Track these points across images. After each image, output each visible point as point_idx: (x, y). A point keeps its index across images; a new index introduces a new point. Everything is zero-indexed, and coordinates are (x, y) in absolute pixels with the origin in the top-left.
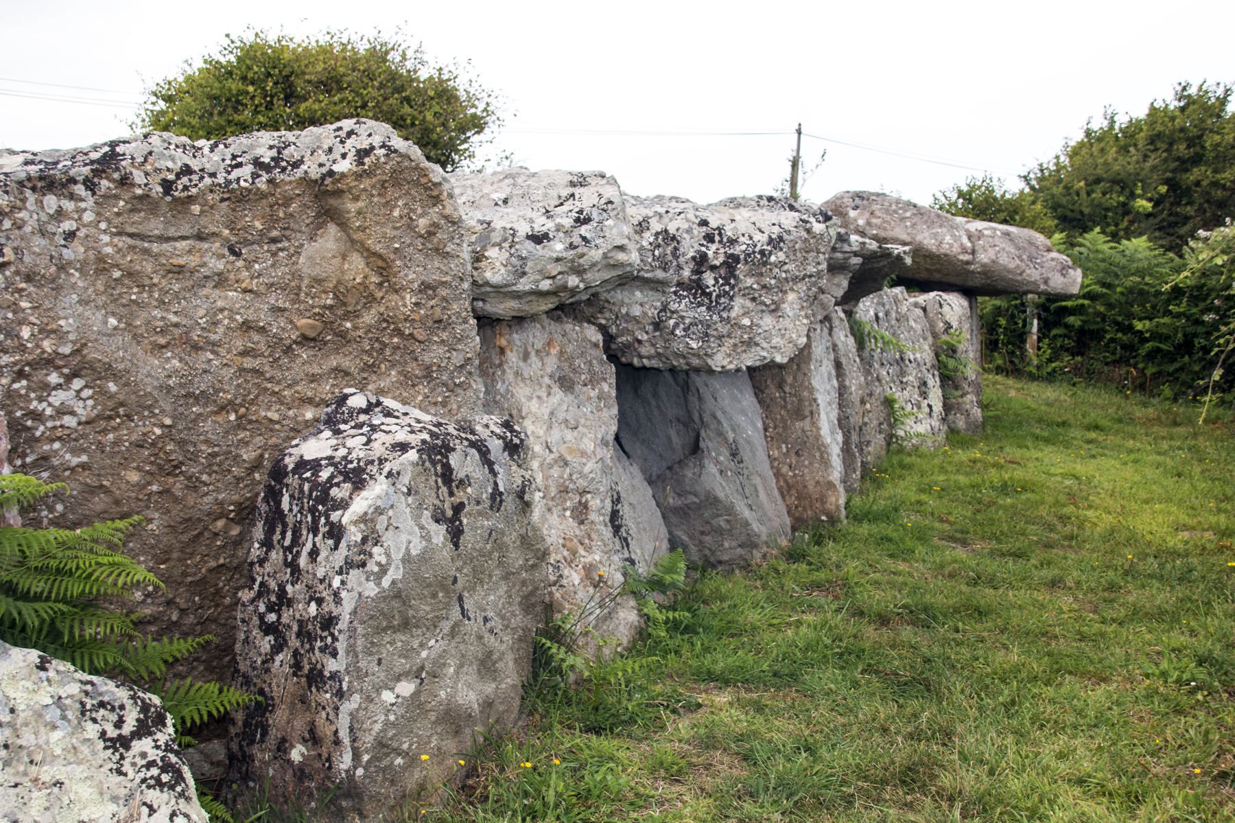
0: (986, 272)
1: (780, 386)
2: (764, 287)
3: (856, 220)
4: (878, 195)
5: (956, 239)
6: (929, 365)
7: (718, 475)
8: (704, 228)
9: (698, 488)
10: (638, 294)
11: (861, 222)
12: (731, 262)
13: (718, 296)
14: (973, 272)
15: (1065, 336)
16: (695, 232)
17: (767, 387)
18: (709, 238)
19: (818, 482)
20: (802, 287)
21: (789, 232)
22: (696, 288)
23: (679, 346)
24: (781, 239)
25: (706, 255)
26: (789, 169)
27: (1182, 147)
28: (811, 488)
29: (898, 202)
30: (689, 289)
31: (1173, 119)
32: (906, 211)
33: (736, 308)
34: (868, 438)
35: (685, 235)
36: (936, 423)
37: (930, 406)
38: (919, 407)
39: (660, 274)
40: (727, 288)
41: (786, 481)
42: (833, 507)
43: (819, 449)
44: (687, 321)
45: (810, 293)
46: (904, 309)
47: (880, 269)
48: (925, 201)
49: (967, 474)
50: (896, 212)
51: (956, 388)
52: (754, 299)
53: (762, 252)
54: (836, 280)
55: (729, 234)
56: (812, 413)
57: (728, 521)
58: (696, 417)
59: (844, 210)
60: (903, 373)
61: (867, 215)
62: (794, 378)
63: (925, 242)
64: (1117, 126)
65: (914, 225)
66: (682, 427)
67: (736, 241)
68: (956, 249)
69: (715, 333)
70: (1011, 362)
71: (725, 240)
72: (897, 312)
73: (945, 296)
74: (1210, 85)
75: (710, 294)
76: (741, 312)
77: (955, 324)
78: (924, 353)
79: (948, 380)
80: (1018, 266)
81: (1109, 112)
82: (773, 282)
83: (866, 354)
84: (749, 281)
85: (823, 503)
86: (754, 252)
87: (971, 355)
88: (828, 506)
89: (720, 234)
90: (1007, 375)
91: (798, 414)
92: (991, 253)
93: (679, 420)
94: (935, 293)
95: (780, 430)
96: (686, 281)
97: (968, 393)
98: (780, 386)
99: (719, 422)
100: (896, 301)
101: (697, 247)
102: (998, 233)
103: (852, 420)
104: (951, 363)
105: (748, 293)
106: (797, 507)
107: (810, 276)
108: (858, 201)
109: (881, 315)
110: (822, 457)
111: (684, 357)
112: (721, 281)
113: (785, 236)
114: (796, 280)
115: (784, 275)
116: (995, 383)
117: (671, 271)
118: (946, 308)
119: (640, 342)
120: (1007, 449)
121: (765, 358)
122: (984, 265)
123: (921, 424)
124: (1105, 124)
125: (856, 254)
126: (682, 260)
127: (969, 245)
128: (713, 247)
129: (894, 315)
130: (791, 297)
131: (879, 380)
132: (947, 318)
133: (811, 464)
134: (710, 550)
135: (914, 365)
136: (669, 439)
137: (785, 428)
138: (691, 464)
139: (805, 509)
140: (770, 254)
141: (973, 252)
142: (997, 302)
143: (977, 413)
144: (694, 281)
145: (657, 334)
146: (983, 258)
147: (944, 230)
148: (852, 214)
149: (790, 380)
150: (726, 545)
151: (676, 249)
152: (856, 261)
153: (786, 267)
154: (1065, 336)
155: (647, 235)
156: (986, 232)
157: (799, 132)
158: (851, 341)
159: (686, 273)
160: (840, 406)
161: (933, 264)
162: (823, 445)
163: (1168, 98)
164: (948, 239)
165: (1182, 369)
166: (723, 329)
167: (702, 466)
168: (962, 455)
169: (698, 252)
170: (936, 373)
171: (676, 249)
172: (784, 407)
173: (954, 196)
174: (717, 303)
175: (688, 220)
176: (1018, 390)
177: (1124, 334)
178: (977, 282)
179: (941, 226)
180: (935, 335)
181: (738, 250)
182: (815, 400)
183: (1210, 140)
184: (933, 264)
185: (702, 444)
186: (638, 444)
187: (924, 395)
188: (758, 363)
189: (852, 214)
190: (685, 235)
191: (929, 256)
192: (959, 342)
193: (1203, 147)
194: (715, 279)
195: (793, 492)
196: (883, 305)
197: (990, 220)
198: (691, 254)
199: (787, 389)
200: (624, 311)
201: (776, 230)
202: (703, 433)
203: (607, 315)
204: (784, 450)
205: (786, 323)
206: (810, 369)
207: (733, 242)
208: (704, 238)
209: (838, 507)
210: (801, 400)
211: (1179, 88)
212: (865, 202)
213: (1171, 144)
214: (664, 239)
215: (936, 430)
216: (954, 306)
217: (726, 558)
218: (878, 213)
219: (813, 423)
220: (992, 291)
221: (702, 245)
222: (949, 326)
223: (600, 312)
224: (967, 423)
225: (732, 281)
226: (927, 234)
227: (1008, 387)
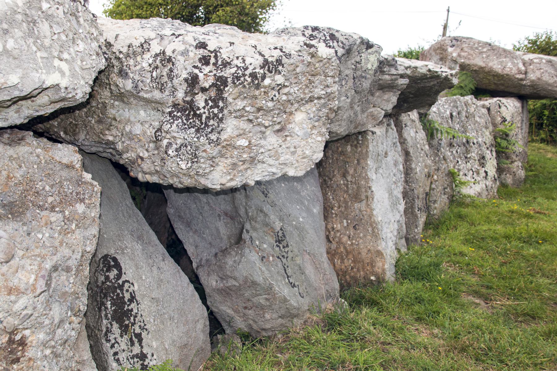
0: (534, 85)
1: (344, 176)
2: (259, 109)
3: (452, 54)
4: (468, 38)
6: (488, 145)
7: (258, 263)
8: (202, 50)
9: (236, 274)
10: (142, 113)
11: (455, 55)
12: (221, 83)
13: (208, 118)
14: (525, 85)
16: (191, 54)
17: (334, 176)
18: (205, 61)
19: (369, 250)
20: (312, 108)
21: (288, 56)
22: (188, 109)
23: (171, 165)
24: (279, 62)
25: (197, 76)
26: (442, 30)
28: (364, 254)
29: (479, 42)
30: (183, 110)
32: (484, 48)
33: (229, 130)
34: (435, 198)
35: (179, 57)
36: (489, 183)
37: (486, 172)
38: (478, 173)
39: (157, 95)
40: (216, 111)
41: (345, 248)
42: (380, 271)
43: (371, 225)
44: (179, 142)
45: (321, 114)
46: (472, 110)
47: (431, 88)
48: (509, 47)
49: (505, 224)
50: (477, 48)
51: (507, 158)
52: (250, 121)
53: (253, 76)
54: (386, 97)
55: (224, 56)
56: (367, 197)
57: (266, 299)
58: (242, 212)
59: (445, 48)
60: (468, 151)
61: (459, 50)
62: (355, 170)
63: (494, 67)
66: (229, 220)
67: (229, 64)
68: (514, 71)
69: (204, 154)
70: (551, 136)
71: (220, 63)
72: (467, 112)
73: (503, 100)
75: (200, 116)
76: (236, 133)
77: (508, 119)
78: (487, 137)
79: (502, 154)
82: (270, 104)
83: (435, 142)
84: (240, 104)
85: (373, 266)
86: (244, 75)
87: (520, 136)
88: (376, 269)
89: (216, 57)
90: (547, 144)
91: (357, 198)
92: (538, 74)
93: (226, 214)
94: (498, 98)
95: (343, 209)
96: (181, 102)
97: (515, 161)
98: (344, 176)
99: (266, 215)
100: (466, 104)
101: (189, 70)
102: (544, 61)
103: (416, 192)
104: (504, 143)
105: (240, 114)
106: (352, 268)
107: (319, 98)
108: (454, 42)
109: (454, 114)
110: (373, 231)
111: (178, 177)
112: (211, 104)
113: (285, 60)
114: (302, 102)
115: (284, 98)
116: (539, 149)
117: (167, 93)
118: (503, 109)
119: (142, 159)
120: (539, 200)
121: (274, 174)
122: (532, 81)
123: (476, 185)
125: (402, 76)
126: (175, 81)
127: (523, 68)
128: (206, 69)
129: (464, 114)
130: (299, 117)
131: (444, 159)
132: (504, 115)
133: (365, 236)
134: (254, 321)
135: (476, 146)
136: (218, 230)
137: (346, 208)
138: (233, 253)
139: (358, 270)
140: (264, 77)
141: (526, 73)
142: (544, 101)
143: (522, 173)
144: (188, 102)
145: (156, 152)
146: (532, 76)
147: (508, 59)
148: (450, 50)
149: (351, 171)
150: (267, 316)
151: (171, 70)
152: (404, 82)
153: (286, 90)
155: (147, 56)
156: (535, 61)
157: (448, 11)
158: (422, 135)
159: (180, 95)
160: (406, 182)
161: (499, 80)
162: (374, 222)
164: (509, 65)
166: (213, 151)
167: (242, 255)
168: (506, 206)
169: (190, 74)
170: (493, 149)
171: (171, 70)
172: (347, 192)
173: (526, 43)
174: (207, 125)
175: (184, 42)
176: (553, 153)
178: (527, 91)
179: (505, 57)
180: (495, 125)
181: (228, 73)
182: (370, 188)
185: (245, 236)
186: (191, 234)
187: (483, 165)
188: (267, 178)
189: (450, 50)
190: (179, 57)
191: (496, 76)
192: (511, 130)
194: (206, 101)
195: (350, 256)
196: (457, 108)
197: (549, 55)
198: (184, 75)
199: (349, 178)
200: (128, 129)
201: (277, 54)
202: (247, 226)
203: (114, 132)
204: (345, 224)
205: (295, 141)
206: (367, 164)
207: (226, 64)
208: (200, 60)
209: (384, 270)
210: (359, 188)
212: (459, 43)
214: (161, 61)
215: (489, 188)
216: (510, 107)
217: (268, 326)
218: (466, 49)
219: (368, 205)
220: (537, 96)
221: (195, 67)
222: (504, 120)
223: (109, 129)
224: (513, 180)
225: (221, 104)
226: (495, 62)
227: (547, 151)
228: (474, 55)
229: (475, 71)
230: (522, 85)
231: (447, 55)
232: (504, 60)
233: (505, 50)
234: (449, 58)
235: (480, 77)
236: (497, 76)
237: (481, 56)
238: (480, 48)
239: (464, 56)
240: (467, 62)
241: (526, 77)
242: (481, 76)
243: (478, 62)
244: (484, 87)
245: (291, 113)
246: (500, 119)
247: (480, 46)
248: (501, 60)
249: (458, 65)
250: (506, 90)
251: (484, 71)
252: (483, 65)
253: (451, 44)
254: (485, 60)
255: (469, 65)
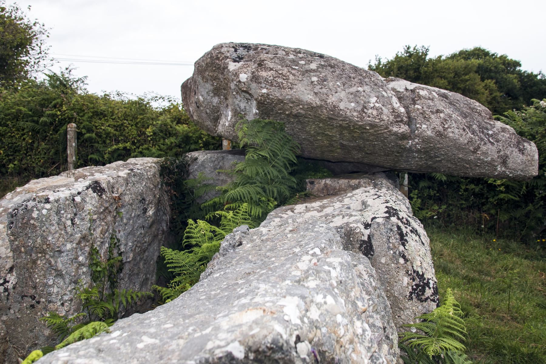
3: (236, 75)
5: (384, 103)
11: (243, 77)
14: (410, 150)
15: (429, 188)
27: (412, 72)
31: (406, 60)
61: (253, 66)
63: (342, 106)
64: (382, 63)
65: (324, 80)
68: (387, 116)
74: (419, 48)
80: (471, 141)
81: (378, 58)
108: (241, 51)
122: (426, 140)
124: (377, 63)
141: (410, 121)
146: (426, 129)
148: (232, 66)
154: (429, 188)
161: (354, 139)
163: (401, 52)
165: (527, 215)
177: (477, 185)
179: (361, 84)
183: (423, 69)
184: (354, 139)
189: (232, 66)
191: (348, 128)
193: (420, 73)
211: (406, 48)
212: (252, 52)
213: (407, 71)
226: (342, 95)
228: (291, 77)
229: (296, 116)
230: (405, 149)
231: (228, 81)
232: (360, 89)
233: (356, 69)
234: (232, 86)
235: (308, 133)
236: (348, 127)
237: (306, 81)
238: (303, 62)
239: (266, 80)
240: (277, 94)
241: (412, 131)
242: (312, 128)
243: (304, 93)
244: (317, 154)
245: (79, 159)
246: (406, 280)
247: (301, 59)
248: (353, 89)
249: (255, 103)
250: (366, 160)
251: (318, 118)
252: (316, 101)
253: (235, 55)
254: (317, 89)
255: (281, 101)
